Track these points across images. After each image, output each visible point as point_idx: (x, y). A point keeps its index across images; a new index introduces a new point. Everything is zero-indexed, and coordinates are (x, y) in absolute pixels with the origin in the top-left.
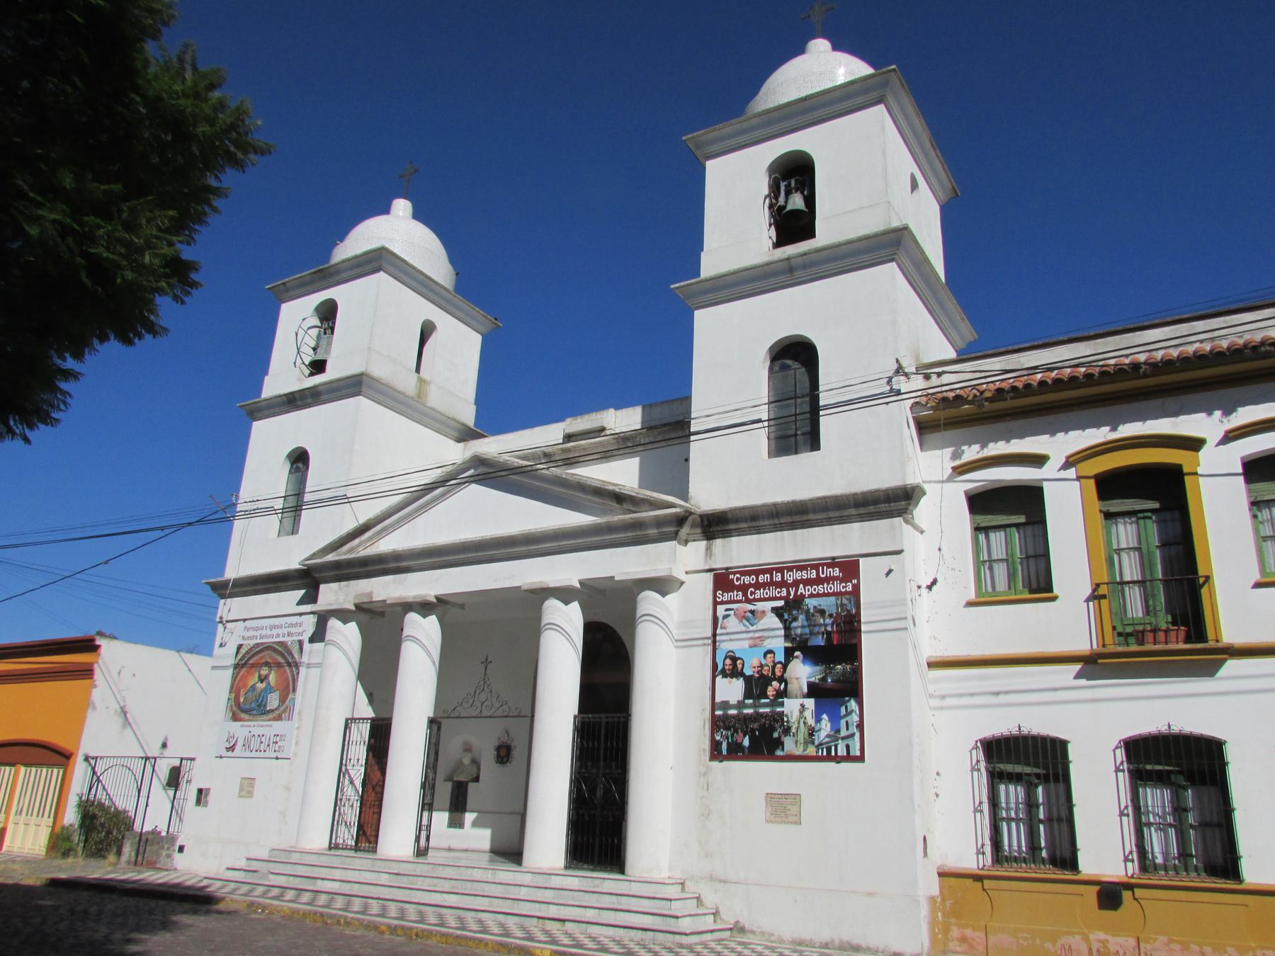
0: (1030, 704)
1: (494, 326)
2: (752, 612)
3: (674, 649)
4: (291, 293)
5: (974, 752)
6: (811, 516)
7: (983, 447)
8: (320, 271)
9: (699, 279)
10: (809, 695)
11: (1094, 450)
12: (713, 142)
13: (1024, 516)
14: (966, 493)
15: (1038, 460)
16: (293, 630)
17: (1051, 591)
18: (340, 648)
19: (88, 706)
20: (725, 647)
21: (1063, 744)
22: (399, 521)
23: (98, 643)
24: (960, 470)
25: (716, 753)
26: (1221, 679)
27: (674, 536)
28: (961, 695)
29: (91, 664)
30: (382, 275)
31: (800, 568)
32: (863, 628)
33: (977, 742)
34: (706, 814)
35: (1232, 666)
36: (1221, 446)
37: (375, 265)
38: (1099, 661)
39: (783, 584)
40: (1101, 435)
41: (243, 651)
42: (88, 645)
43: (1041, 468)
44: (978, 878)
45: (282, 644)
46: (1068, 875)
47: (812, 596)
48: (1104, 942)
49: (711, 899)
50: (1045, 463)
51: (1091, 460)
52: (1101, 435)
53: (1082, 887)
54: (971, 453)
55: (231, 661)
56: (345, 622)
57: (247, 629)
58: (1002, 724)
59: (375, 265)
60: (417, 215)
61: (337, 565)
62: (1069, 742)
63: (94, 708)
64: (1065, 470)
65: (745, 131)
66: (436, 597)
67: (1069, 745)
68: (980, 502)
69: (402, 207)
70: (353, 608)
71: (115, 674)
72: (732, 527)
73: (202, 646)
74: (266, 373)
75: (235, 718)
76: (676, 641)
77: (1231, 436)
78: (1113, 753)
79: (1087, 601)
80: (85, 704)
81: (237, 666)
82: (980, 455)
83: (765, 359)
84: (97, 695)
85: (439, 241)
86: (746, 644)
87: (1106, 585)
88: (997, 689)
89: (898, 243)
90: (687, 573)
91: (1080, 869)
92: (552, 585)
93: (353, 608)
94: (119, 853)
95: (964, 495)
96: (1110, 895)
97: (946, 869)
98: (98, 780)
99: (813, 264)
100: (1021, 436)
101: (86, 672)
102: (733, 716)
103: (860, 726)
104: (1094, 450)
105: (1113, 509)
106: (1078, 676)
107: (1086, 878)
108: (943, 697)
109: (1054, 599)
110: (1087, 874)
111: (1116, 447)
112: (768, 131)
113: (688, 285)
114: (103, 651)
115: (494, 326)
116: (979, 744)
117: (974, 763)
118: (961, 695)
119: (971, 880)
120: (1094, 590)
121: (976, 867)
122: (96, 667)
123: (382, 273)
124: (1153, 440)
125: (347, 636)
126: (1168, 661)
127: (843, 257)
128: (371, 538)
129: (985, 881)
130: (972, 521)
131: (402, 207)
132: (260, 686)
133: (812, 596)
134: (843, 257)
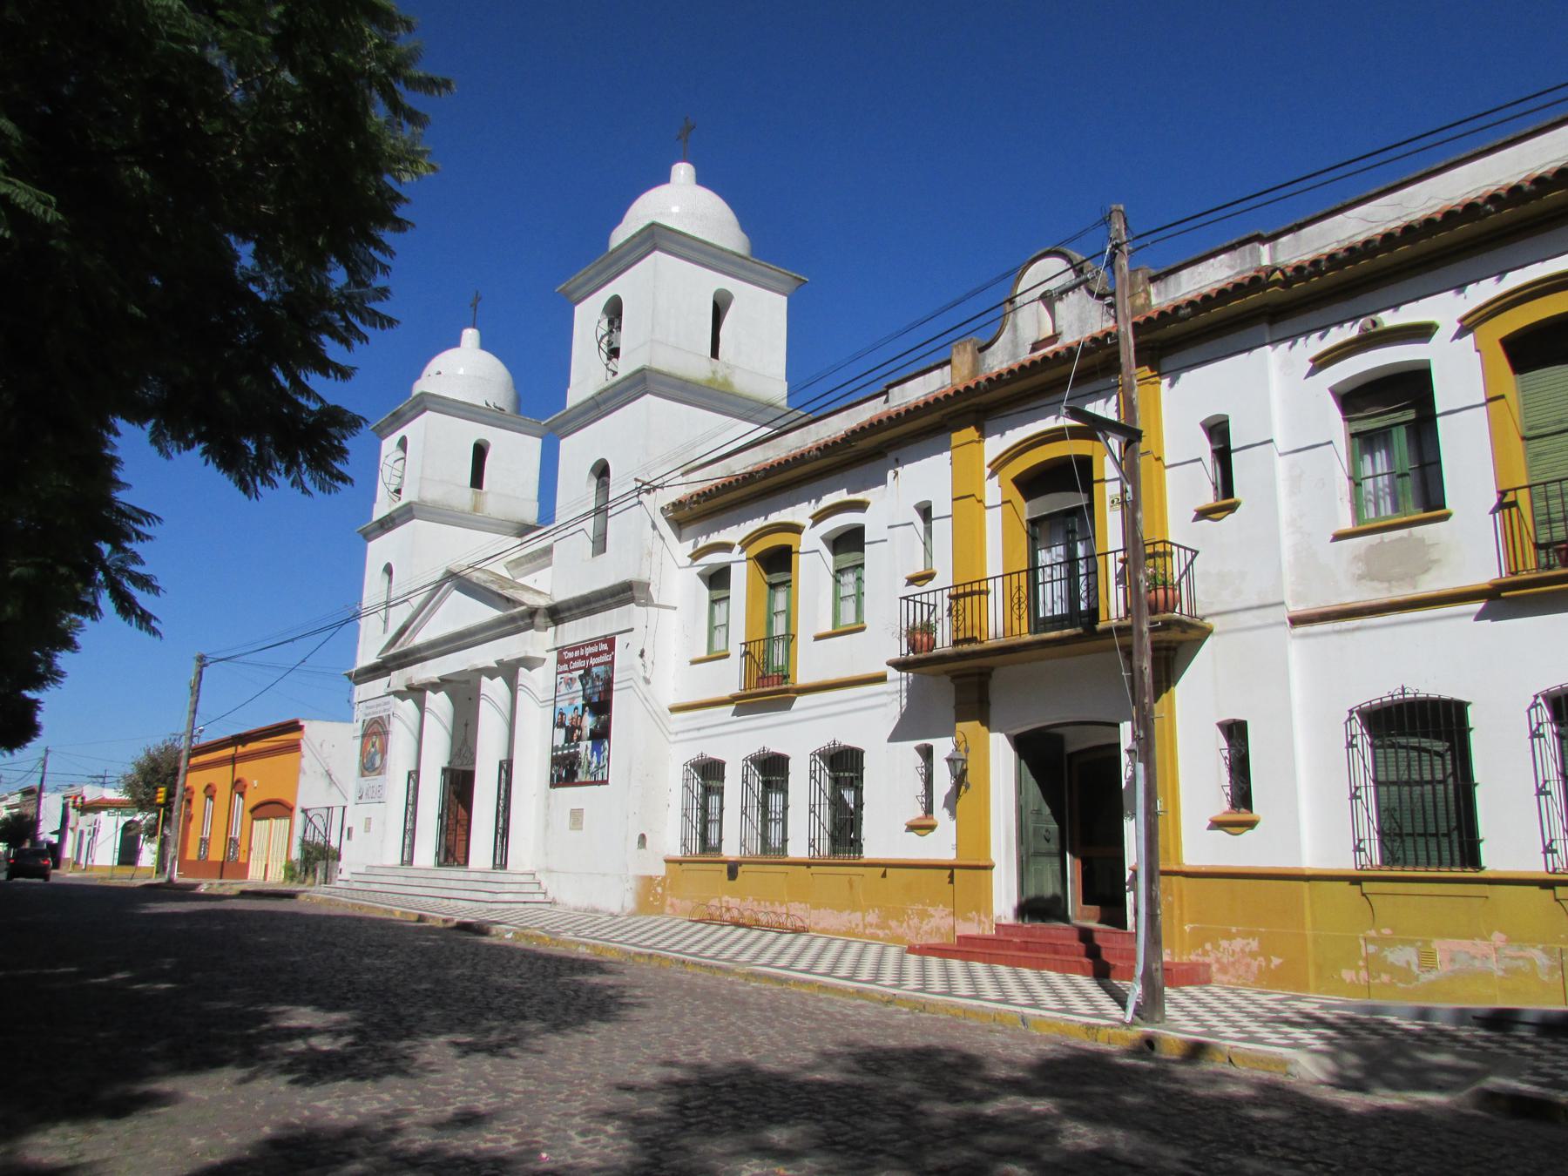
0: (738, 732)
1: (798, 283)
2: (571, 679)
3: (540, 710)
4: (385, 432)
5: (1533, 711)
6: (594, 606)
7: (817, 502)
8: (394, 414)
9: (564, 411)
10: (589, 739)
11: (1491, 307)
12: (578, 288)
13: (1413, 411)
14: (1333, 391)
15: (1422, 332)
16: (386, 707)
17: (1443, 506)
18: (400, 718)
19: (299, 771)
20: (559, 705)
21: (862, 752)
22: (421, 621)
23: (301, 723)
24: (1322, 362)
25: (553, 785)
26: (794, 711)
27: (531, 626)
28: (689, 731)
29: (299, 740)
30: (428, 414)
31: (592, 645)
32: (615, 687)
33: (1536, 697)
34: (547, 826)
35: (801, 701)
36: (1310, 378)
37: (421, 407)
38: (1503, 594)
39: (583, 658)
40: (758, 523)
41: (366, 723)
42: (294, 727)
43: (864, 512)
44: (1355, 880)
45: (381, 717)
46: (1469, 873)
47: (596, 665)
48: (728, 902)
49: (545, 884)
50: (1433, 334)
51: (755, 544)
52: (758, 523)
53: (1487, 887)
54: (703, 542)
55: (360, 733)
56: (492, 678)
57: (367, 707)
58: (1380, 689)
59: (421, 407)
60: (702, 180)
61: (395, 657)
62: (1469, 704)
63: (305, 773)
64: (1460, 338)
65: (609, 266)
66: (440, 678)
67: (1469, 709)
68: (1352, 399)
69: (683, 172)
70: (405, 689)
71: (317, 746)
72: (562, 615)
73: (348, 719)
74: (568, 386)
75: (363, 775)
76: (631, 687)
77: (818, 518)
78: (1526, 714)
79: (1493, 512)
80: (298, 771)
81: (364, 736)
82: (817, 510)
83: (589, 479)
84: (305, 763)
85: (721, 200)
86: (567, 703)
87: (1526, 490)
88: (698, 726)
89: (644, 380)
90: (547, 651)
91: (1483, 864)
92: (480, 666)
93: (405, 689)
94: (315, 877)
95: (1201, 428)
96: (733, 870)
97: (670, 858)
98: (310, 820)
99: (605, 401)
100: (779, 509)
101: (295, 747)
102: (560, 756)
103: (608, 759)
104: (1491, 307)
105: (773, 581)
106: (1480, 616)
107: (1492, 876)
108: (677, 733)
109: (1446, 517)
110: (1493, 871)
111: (1522, 297)
112: (604, 277)
113: (554, 420)
114: (305, 729)
115: (798, 283)
116: (1540, 700)
117: (1534, 728)
118: (689, 731)
119: (1348, 883)
120: (1500, 500)
121: (1543, 869)
122: (302, 742)
123: (428, 412)
124: (1534, 288)
125: (439, 702)
126: (752, 703)
127: (621, 393)
128: (409, 636)
129: (1364, 884)
130: (710, 595)
131: (683, 172)
132: (373, 750)
133: (596, 665)
134: (621, 393)
